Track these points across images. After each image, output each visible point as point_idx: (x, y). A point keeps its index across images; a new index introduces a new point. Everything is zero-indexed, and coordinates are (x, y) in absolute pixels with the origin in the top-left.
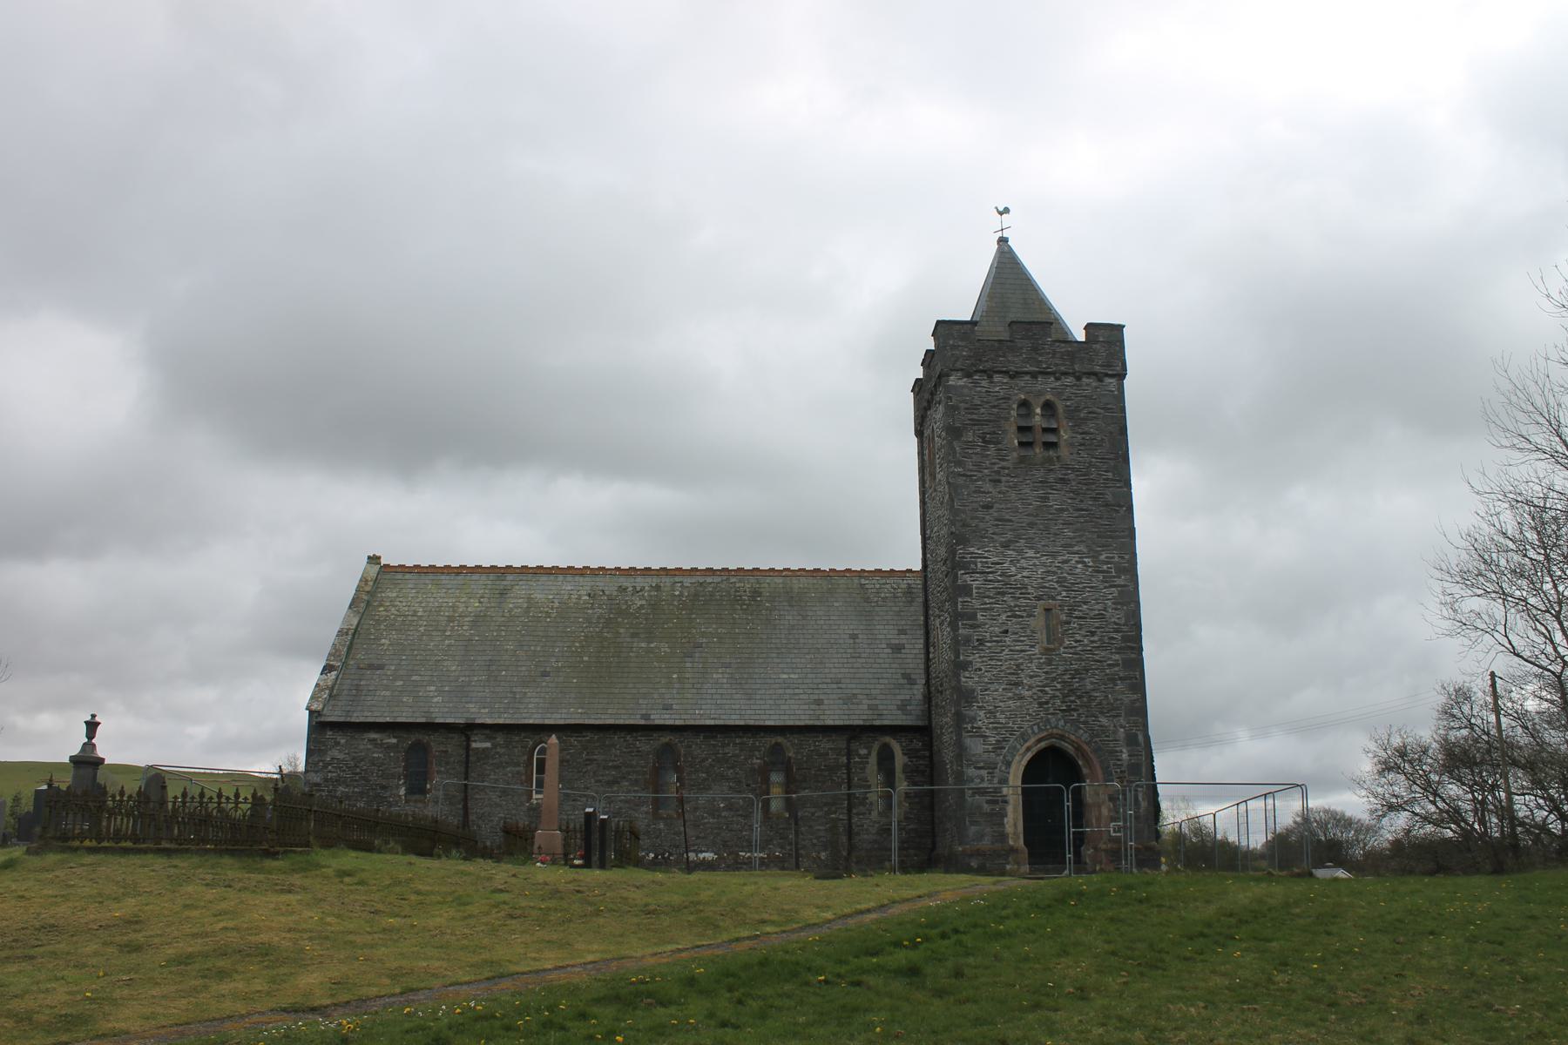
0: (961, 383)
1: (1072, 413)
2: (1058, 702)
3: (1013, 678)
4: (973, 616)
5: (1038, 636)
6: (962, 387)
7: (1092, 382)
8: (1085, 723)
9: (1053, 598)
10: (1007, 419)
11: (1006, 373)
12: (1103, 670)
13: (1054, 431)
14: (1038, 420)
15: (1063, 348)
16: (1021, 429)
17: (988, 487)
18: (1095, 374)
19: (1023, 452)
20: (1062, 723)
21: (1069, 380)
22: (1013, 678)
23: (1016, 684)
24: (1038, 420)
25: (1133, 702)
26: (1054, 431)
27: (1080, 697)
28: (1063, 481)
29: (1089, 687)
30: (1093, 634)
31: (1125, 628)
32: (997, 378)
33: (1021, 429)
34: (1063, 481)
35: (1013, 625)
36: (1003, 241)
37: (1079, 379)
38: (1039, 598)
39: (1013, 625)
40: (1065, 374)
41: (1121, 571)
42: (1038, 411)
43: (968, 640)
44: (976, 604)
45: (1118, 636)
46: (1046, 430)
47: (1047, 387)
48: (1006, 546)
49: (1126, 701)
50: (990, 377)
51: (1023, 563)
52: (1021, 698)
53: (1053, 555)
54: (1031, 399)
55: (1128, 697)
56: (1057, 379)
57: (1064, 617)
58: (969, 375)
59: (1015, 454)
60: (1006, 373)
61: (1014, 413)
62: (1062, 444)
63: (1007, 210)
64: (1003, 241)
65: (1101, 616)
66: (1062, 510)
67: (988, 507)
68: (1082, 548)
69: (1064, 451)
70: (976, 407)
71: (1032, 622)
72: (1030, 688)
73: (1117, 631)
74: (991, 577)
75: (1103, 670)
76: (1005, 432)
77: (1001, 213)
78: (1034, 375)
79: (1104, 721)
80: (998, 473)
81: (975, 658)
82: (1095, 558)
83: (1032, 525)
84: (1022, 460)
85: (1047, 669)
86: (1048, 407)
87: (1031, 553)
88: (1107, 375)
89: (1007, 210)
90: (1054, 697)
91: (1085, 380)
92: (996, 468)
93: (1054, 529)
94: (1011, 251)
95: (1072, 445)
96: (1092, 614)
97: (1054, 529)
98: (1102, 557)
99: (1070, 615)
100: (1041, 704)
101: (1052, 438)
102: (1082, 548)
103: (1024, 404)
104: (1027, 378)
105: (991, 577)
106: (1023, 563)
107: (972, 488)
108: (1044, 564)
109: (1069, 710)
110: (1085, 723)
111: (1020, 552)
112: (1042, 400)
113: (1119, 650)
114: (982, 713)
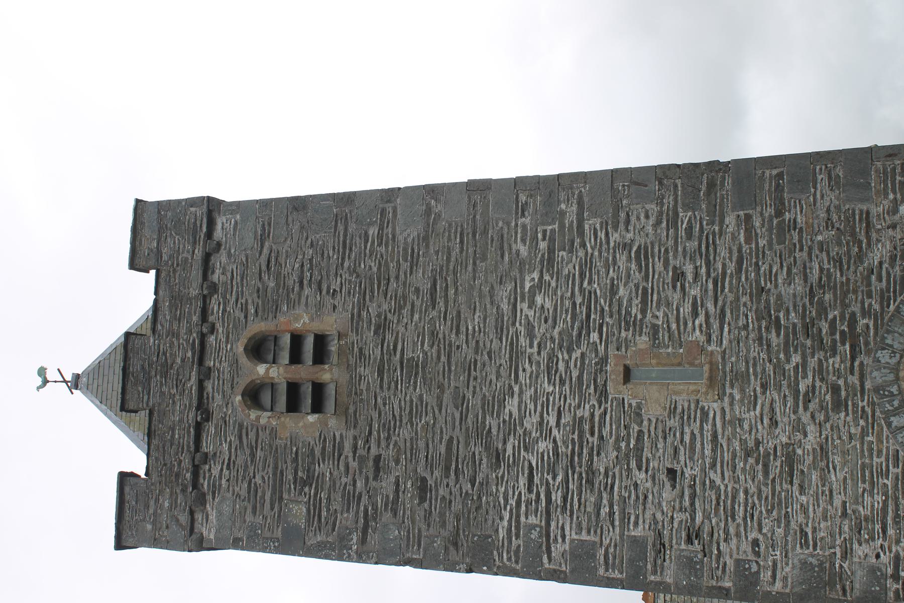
0: (213, 517)
1: (270, 306)
2: (834, 362)
3: (776, 466)
4: (637, 543)
5: (682, 401)
6: (220, 514)
7: (220, 259)
8: (884, 300)
9: (604, 361)
10: (274, 433)
11: (199, 427)
12: (760, 254)
13: (297, 340)
14: (276, 372)
15: (166, 314)
16: (293, 406)
17: (386, 485)
18: (207, 258)
19: (330, 405)
20: (884, 356)
21: (214, 304)
22: (776, 466)
23: (790, 460)
24: (276, 372)
25: (834, 182)
26: (297, 340)
27: (823, 311)
28: (382, 327)
29: (798, 287)
30: (679, 275)
31: (669, 200)
32: (208, 446)
33: (293, 406)
34: (382, 327)
35: (660, 459)
36: (76, 383)
37: (214, 288)
38: (603, 394)
39: (660, 459)
40: (204, 314)
41: (550, 211)
42: (261, 369)
43: (690, 565)
44: (612, 535)
45: (684, 216)
46: (296, 357)
47: (228, 347)
48: (497, 458)
49: (831, 197)
50: (206, 458)
51: (530, 422)
52: (823, 450)
53: (516, 354)
54: (242, 383)
55: (569, 532)
56: (213, 329)
57: (643, 341)
58: (201, 500)
59: (332, 422)
60: (199, 427)
61: (265, 417)
62: (318, 326)
63: (42, 372)
64: (76, 383)
65: (643, 256)
66: (433, 334)
67: (423, 488)
68: (503, 293)
69: (330, 324)
70: (253, 490)
71: (653, 411)
72: (799, 427)
73: (674, 222)
74: (557, 497)
75: (760, 254)
76: (293, 440)
77: (45, 382)
78: (205, 374)
79: (879, 253)
80: (362, 461)
81: (734, 550)
82: (523, 266)
83: (460, 401)
84: (341, 410)
85: (755, 384)
86: (258, 349)
87: (512, 406)
88: (209, 234)
89: (42, 372)
90: (820, 371)
91: (215, 278)
92: (354, 465)
93: (467, 352)
94: (87, 372)
95: (320, 306)
96: (637, 276)
97: (467, 352)
98: (524, 251)
99: (636, 326)
100: (839, 405)
101: (309, 345)
102: (503, 293)
103: (254, 395)
104: (209, 386)
105: (557, 497)
106: (530, 422)
107: (387, 516)
108: (535, 378)
109: (852, 337)
110: (884, 300)
111: (510, 427)
112: (244, 360)
113: (716, 214)
114: (860, 551)
